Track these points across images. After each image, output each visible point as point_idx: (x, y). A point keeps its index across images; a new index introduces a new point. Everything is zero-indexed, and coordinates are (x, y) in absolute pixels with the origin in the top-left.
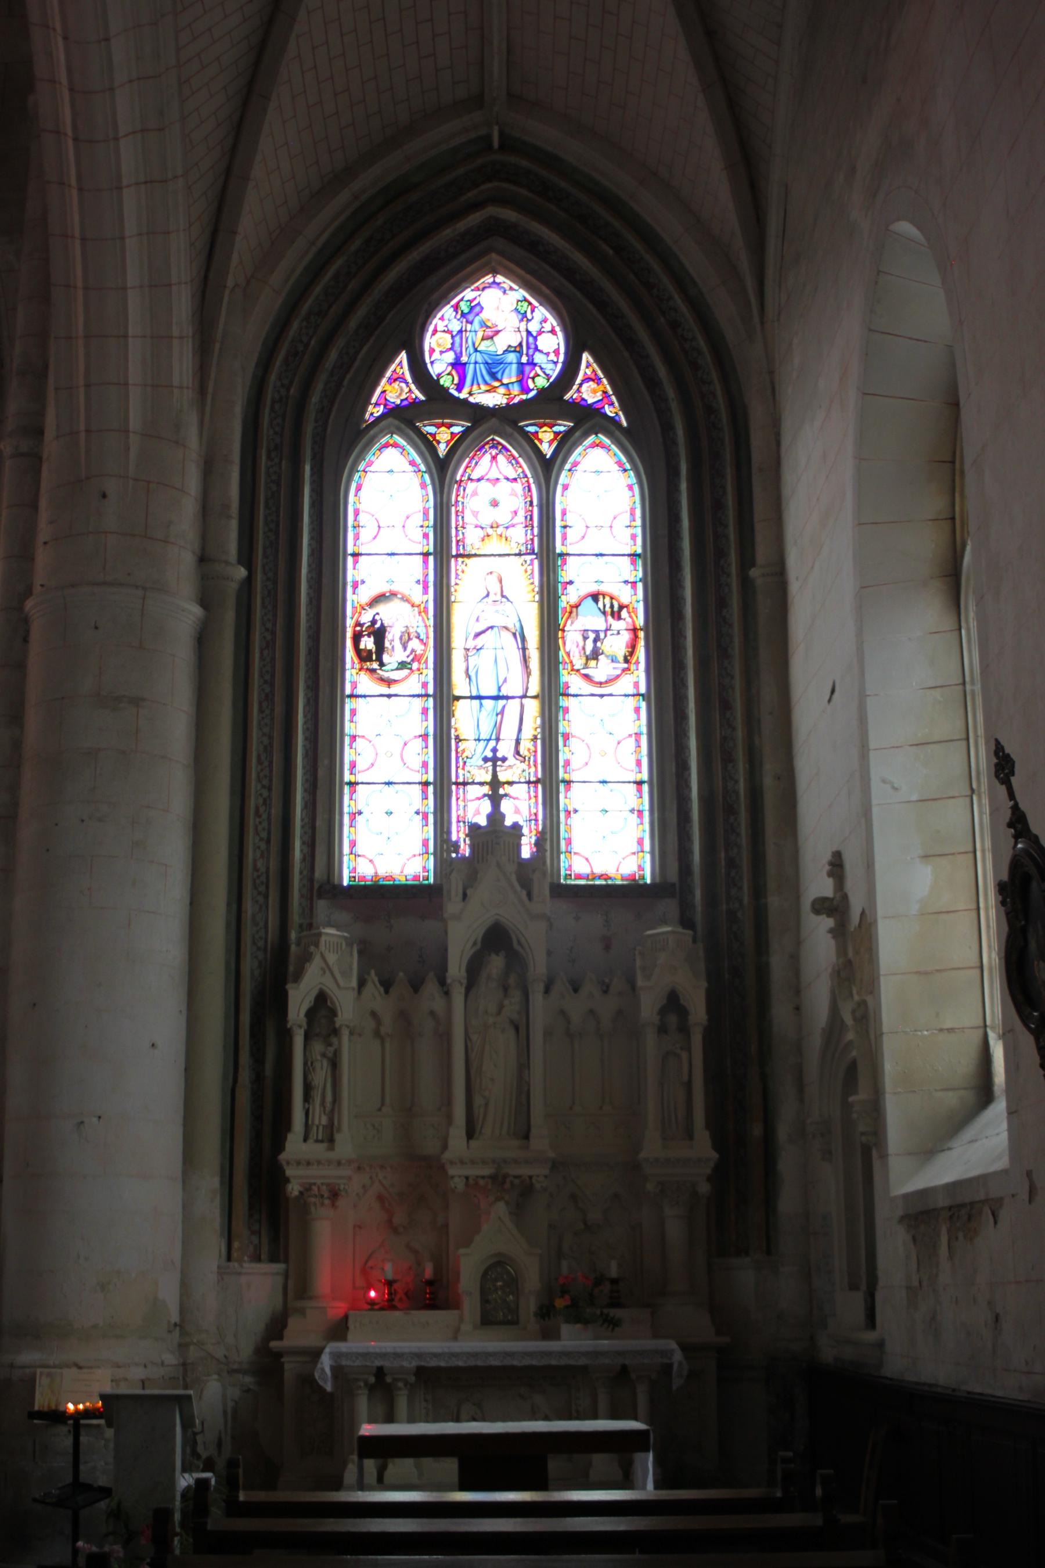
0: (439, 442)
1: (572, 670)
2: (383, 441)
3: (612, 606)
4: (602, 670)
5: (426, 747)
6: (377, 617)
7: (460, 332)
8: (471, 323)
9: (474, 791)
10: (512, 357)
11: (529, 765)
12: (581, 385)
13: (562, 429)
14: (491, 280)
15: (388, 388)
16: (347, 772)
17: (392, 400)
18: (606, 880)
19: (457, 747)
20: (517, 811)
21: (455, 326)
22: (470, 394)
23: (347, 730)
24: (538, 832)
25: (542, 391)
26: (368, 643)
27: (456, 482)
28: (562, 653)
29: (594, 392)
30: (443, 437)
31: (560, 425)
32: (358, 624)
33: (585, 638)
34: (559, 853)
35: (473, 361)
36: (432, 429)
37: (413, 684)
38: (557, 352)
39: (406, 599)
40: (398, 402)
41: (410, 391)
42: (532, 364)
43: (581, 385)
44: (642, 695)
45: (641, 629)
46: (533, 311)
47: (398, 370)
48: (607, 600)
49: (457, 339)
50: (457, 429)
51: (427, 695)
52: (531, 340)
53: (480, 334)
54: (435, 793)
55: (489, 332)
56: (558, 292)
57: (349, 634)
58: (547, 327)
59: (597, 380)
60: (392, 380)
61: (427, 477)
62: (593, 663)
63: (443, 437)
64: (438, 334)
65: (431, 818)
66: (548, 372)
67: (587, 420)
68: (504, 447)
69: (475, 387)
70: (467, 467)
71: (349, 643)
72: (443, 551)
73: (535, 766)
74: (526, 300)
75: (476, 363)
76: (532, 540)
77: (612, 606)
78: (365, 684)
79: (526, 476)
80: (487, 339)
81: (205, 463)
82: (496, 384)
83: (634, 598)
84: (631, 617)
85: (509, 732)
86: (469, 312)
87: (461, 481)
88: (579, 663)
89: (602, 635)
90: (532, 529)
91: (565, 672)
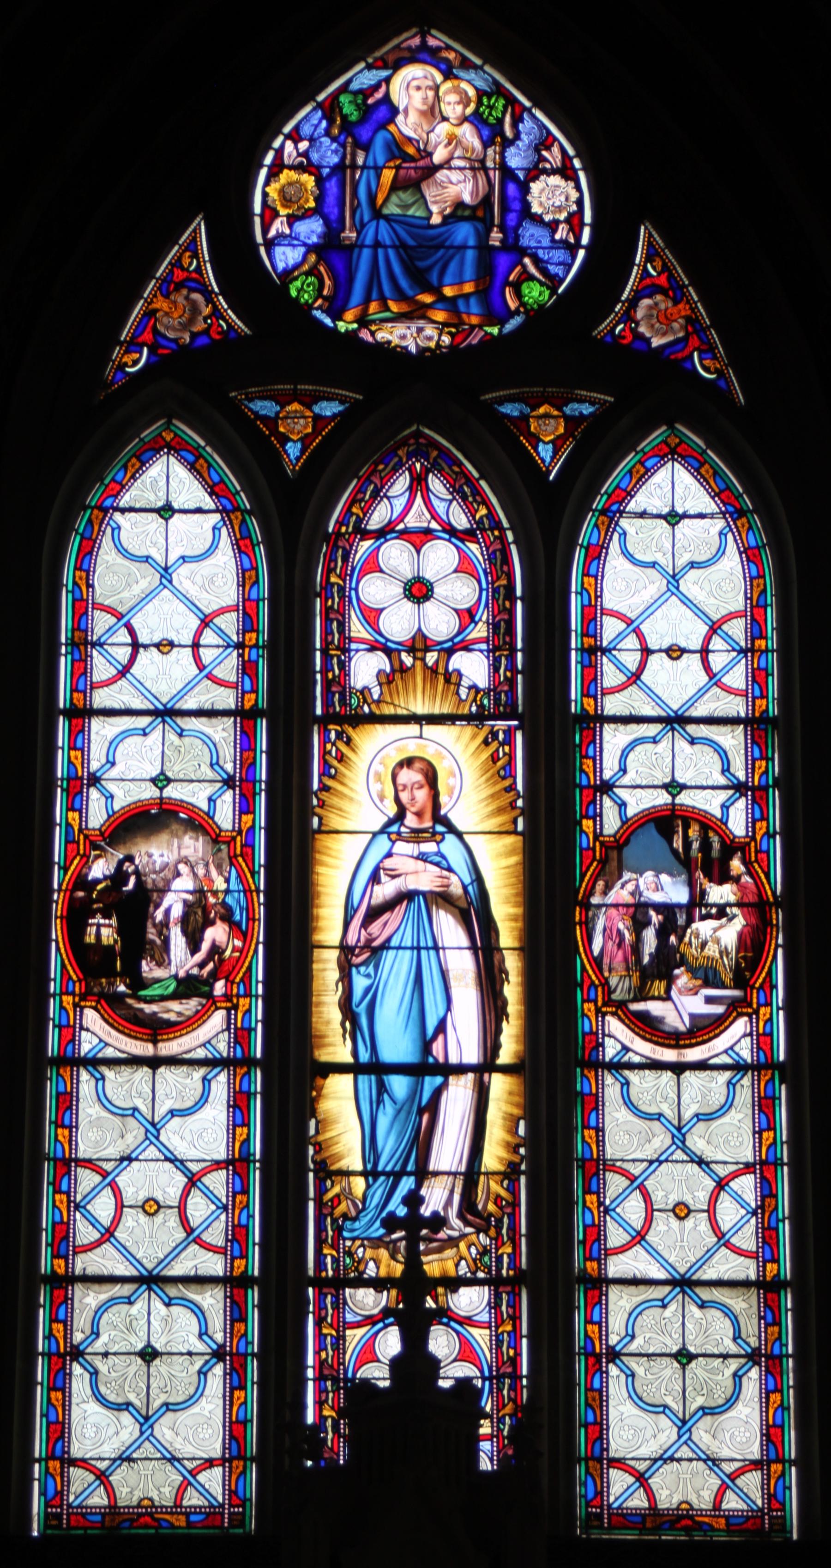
0: (284, 439)
1: (608, 1002)
2: (147, 434)
3: (706, 846)
4: (683, 1005)
5: (245, 1191)
6: (129, 868)
7: (339, 169)
8: (366, 147)
9: (366, 1300)
10: (464, 232)
11: (498, 1240)
13: (587, 409)
14: (416, 41)
15: (161, 304)
16: (45, 1253)
17: (171, 335)
18: (687, 1530)
19: (321, 1190)
20: (467, 1353)
21: (328, 154)
22: (363, 321)
23: (49, 1146)
24: (518, 1407)
25: (536, 315)
26: (104, 931)
27: (327, 537)
28: (582, 960)
29: (667, 319)
30: (296, 428)
31: (581, 401)
32: (82, 882)
33: (639, 925)
34: (572, 1459)
35: (369, 240)
36: (266, 407)
37: (212, 1033)
38: (575, 221)
39: (199, 823)
41: (217, 313)
42: (514, 249)
44: (780, 1067)
45: (777, 904)
46: (517, 120)
47: (186, 262)
48: (694, 832)
49: (332, 186)
51: (248, 1062)
52: (512, 189)
53: (388, 175)
54: (263, 1307)
55: (410, 171)
57: (58, 905)
58: (553, 157)
59: (675, 293)
60: (167, 287)
61: (254, 525)
62: (659, 987)
63: (296, 428)
64: (286, 176)
65: (253, 1369)
66: (553, 269)
67: (642, 405)
68: (445, 454)
69: (373, 307)
70: (352, 501)
71: (57, 931)
72: (293, 705)
73: (514, 1241)
74: (499, 90)
75: (377, 244)
76: (512, 682)
77: (706, 846)
78: (96, 1032)
79: (498, 525)
80: (405, 188)
81: (90, 553)
82: (428, 299)
83: (761, 826)
84: (750, 872)
85: (448, 1151)
86: (362, 121)
87: (338, 534)
88: (620, 984)
89: (681, 920)
90: (512, 658)
91: (589, 1007)
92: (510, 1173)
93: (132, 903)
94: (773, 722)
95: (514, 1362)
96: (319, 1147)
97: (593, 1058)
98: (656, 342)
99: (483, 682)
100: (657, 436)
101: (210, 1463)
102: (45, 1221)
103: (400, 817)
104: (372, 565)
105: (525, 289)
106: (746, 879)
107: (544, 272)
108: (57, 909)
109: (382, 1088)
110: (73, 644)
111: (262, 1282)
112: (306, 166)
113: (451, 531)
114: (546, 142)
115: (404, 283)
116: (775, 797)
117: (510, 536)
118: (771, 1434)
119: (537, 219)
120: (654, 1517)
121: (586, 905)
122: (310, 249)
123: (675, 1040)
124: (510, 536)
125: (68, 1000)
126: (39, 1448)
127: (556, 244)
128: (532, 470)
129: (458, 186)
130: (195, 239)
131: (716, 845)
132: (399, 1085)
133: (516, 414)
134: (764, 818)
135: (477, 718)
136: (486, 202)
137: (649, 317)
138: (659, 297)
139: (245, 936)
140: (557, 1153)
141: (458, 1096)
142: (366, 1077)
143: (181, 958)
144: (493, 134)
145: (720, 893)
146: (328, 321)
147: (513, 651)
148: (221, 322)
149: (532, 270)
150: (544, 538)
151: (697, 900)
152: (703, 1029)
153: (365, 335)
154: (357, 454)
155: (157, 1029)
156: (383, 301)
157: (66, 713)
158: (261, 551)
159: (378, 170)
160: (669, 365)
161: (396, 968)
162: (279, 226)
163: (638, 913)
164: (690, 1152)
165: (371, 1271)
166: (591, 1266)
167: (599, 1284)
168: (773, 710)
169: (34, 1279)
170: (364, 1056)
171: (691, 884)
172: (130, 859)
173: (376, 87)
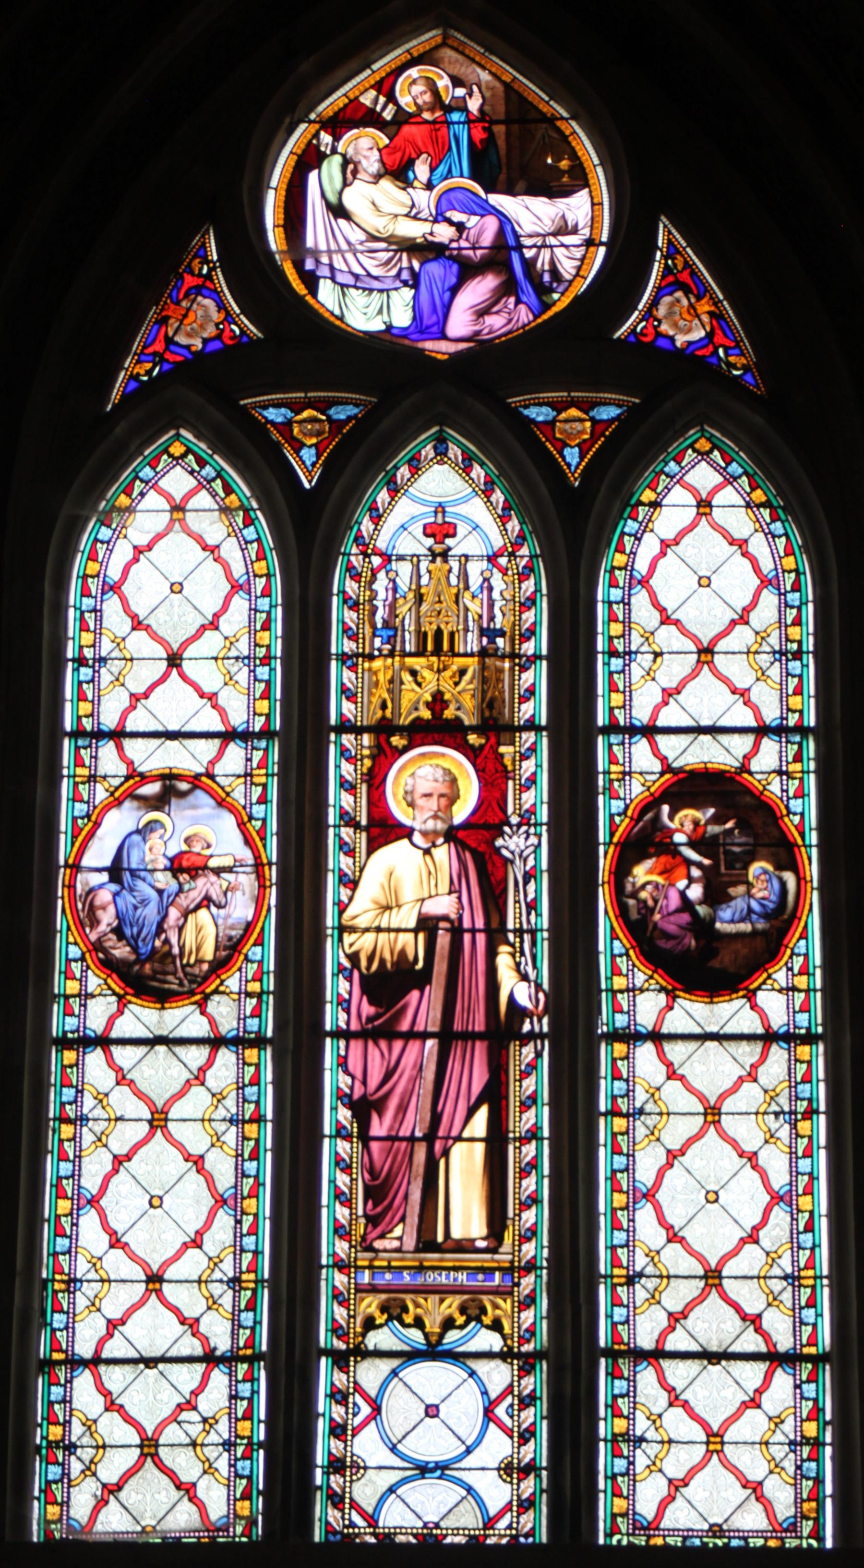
12: (655, 303)
40: (198, 344)
41: (229, 318)
43: (655, 303)
50: (340, 413)
56: (390, 43)
97: (342, 1043)
98: (681, 340)
130: (204, 244)
133: (280, 420)
137: (670, 314)
138: (679, 294)
142: (477, 1029)
148: (234, 327)
160: (692, 364)
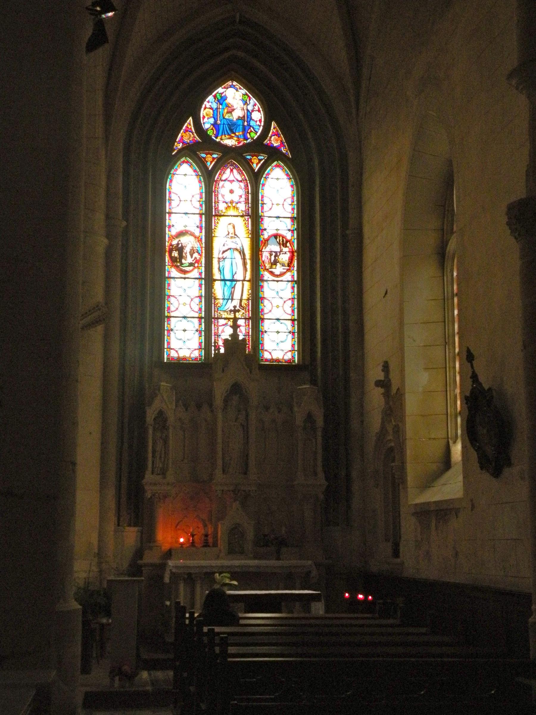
0: (207, 162)
3: (283, 241)
4: (278, 269)
5: (201, 302)
7: (217, 108)
8: (221, 104)
10: (240, 122)
15: (184, 134)
19: (215, 302)
22: (221, 139)
26: (175, 254)
28: (260, 261)
32: (171, 245)
33: (271, 255)
36: (203, 155)
37: (195, 274)
38: (260, 121)
39: (192, 234)
41: (194, 137)
44: (295, 281)
48: (281, 238)
49: (215, 112)
52: (249, 113)
53: (226, 111)
54: (205, 322)
55: (230, 109)
58: (256, 108)
59: (278, 135)
60: (186, 131)
61: (202, 178)
62: (274, 266)
64: (207, 109)
65: (203, 333)
66: (256, 130)
69: (223, 136)
70: (220, 174)
71: (167, 254)
72: (209, 213)
74: (247, 94)
76: (248, 209)
77: (283, 241)
78: (174, 273)
79: (246, 180)
82: (233, 135)
88: (268, 266)
89: (278, 254)
92: (248, 299)
93: (180, 249)
94: (295, 218)
95: (248, 333)
96: (214, 294)
99: (244, 209)
100: (275, 163)
101: (196, 349)
102: (166, 307)
103: (228, 234)
104: (223, 186)
105: (251, 133)
106: (290, 247)
107: (255, 130)
108: (167, 250)
109: (225, 284)
110: (169, 200)
111: (204, 318)
112: (211, 108)
113: (238, 180)
114: (255, 105)
115: (229, 132)
116: (295, 232)
117: (248, 182)
118: (293, 346)
119: (253, 120)
120: (272, 360)
121: (261, 251)
122: (212, 124)
123: (277, 276)
124: (248, 182)
125: (169, 267)
126: (166, 347)
127: (256, 125)
128: (253, 170)
129: (238, 114)
131: (285, 241)
132: (228, 283)
134: (293, 236)
135: (242, 216)
136: (244, 116)
139: (201, 255)
140: (256, 298)
141: (239, 284)
143: (189, 260)
144: (245, 103)
145: (285, 249)
146: (215, 139)
147: (249, 203)
149: (252, 130)
150: (255, 179)
151: (281, 251)
152: (282, 274)
153: (222, 142)
154: (220, 164)
155: (185, 272)
156: (225, 135)
157: (168, 213)
158: (203, 183)
159: (224, 109)
161: (227, 263)
162: (206, 120)
163: (271, 253)
164: (280, 297)
165: (223, 316)
166: (262, 316)
167: (263, 320)
168: (295, 216)
169: (165, 317)
170: (222, 278)
171: (280, 248)
172: (180, 241)
173: (223, 93)
